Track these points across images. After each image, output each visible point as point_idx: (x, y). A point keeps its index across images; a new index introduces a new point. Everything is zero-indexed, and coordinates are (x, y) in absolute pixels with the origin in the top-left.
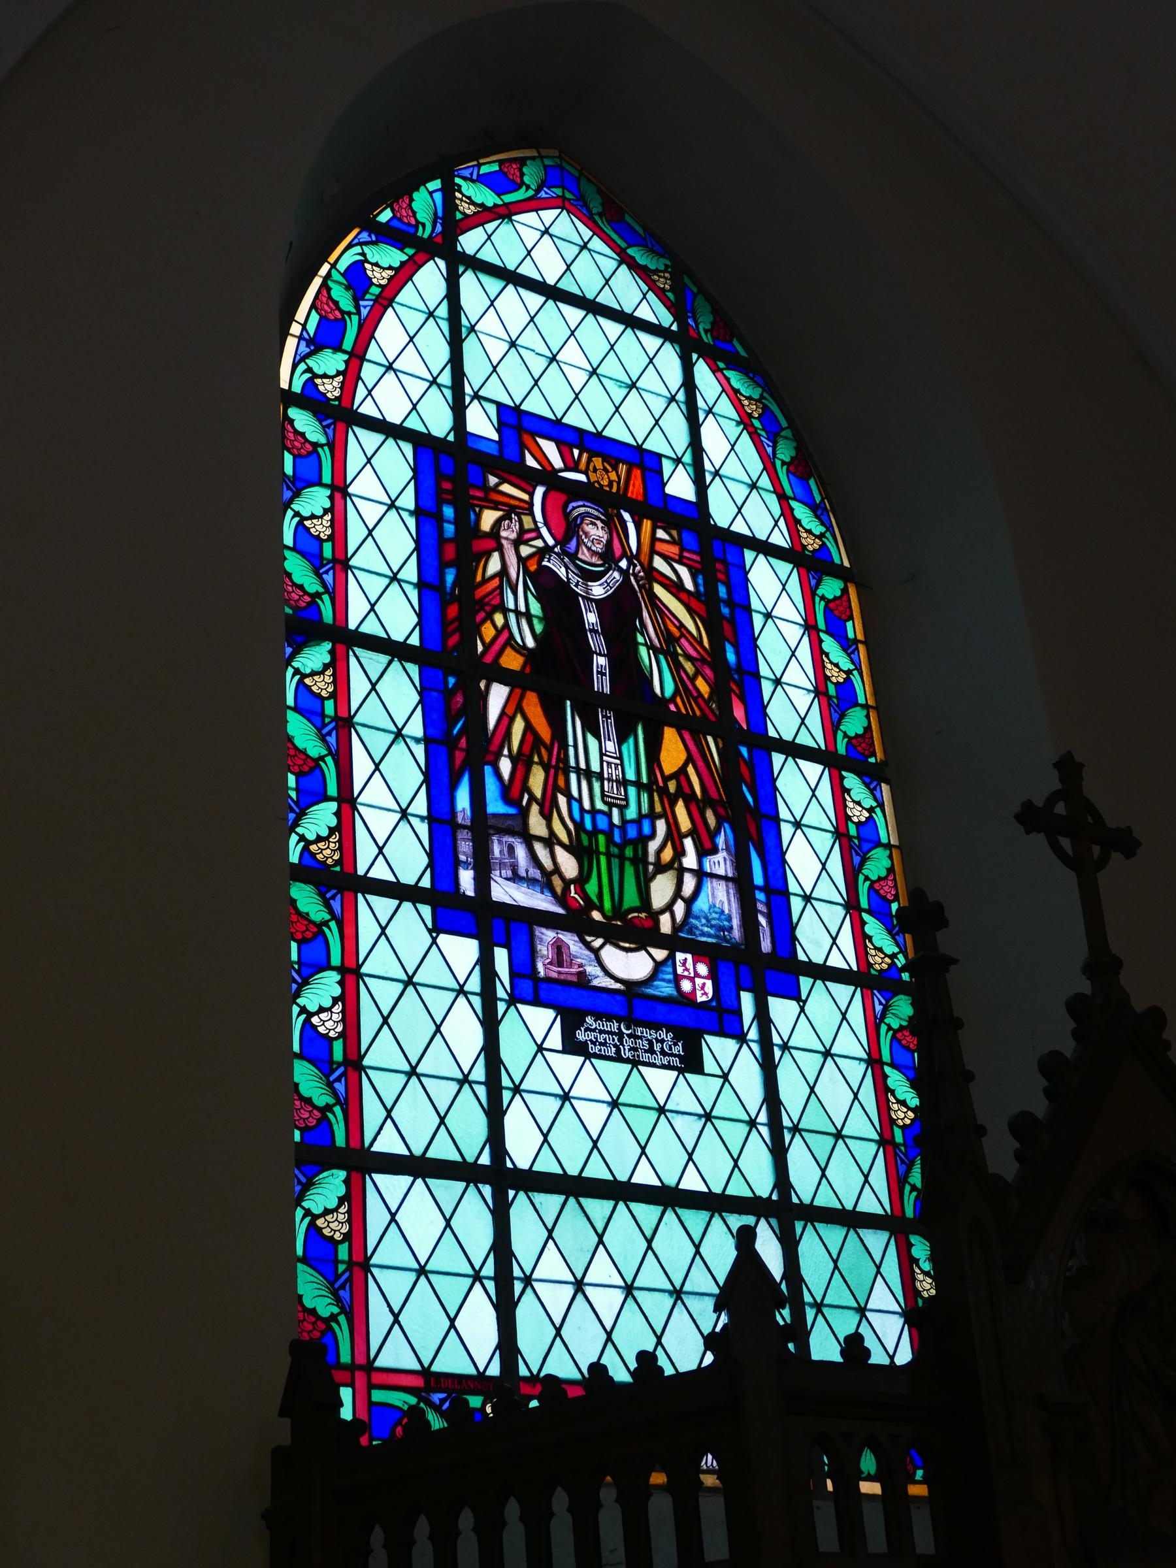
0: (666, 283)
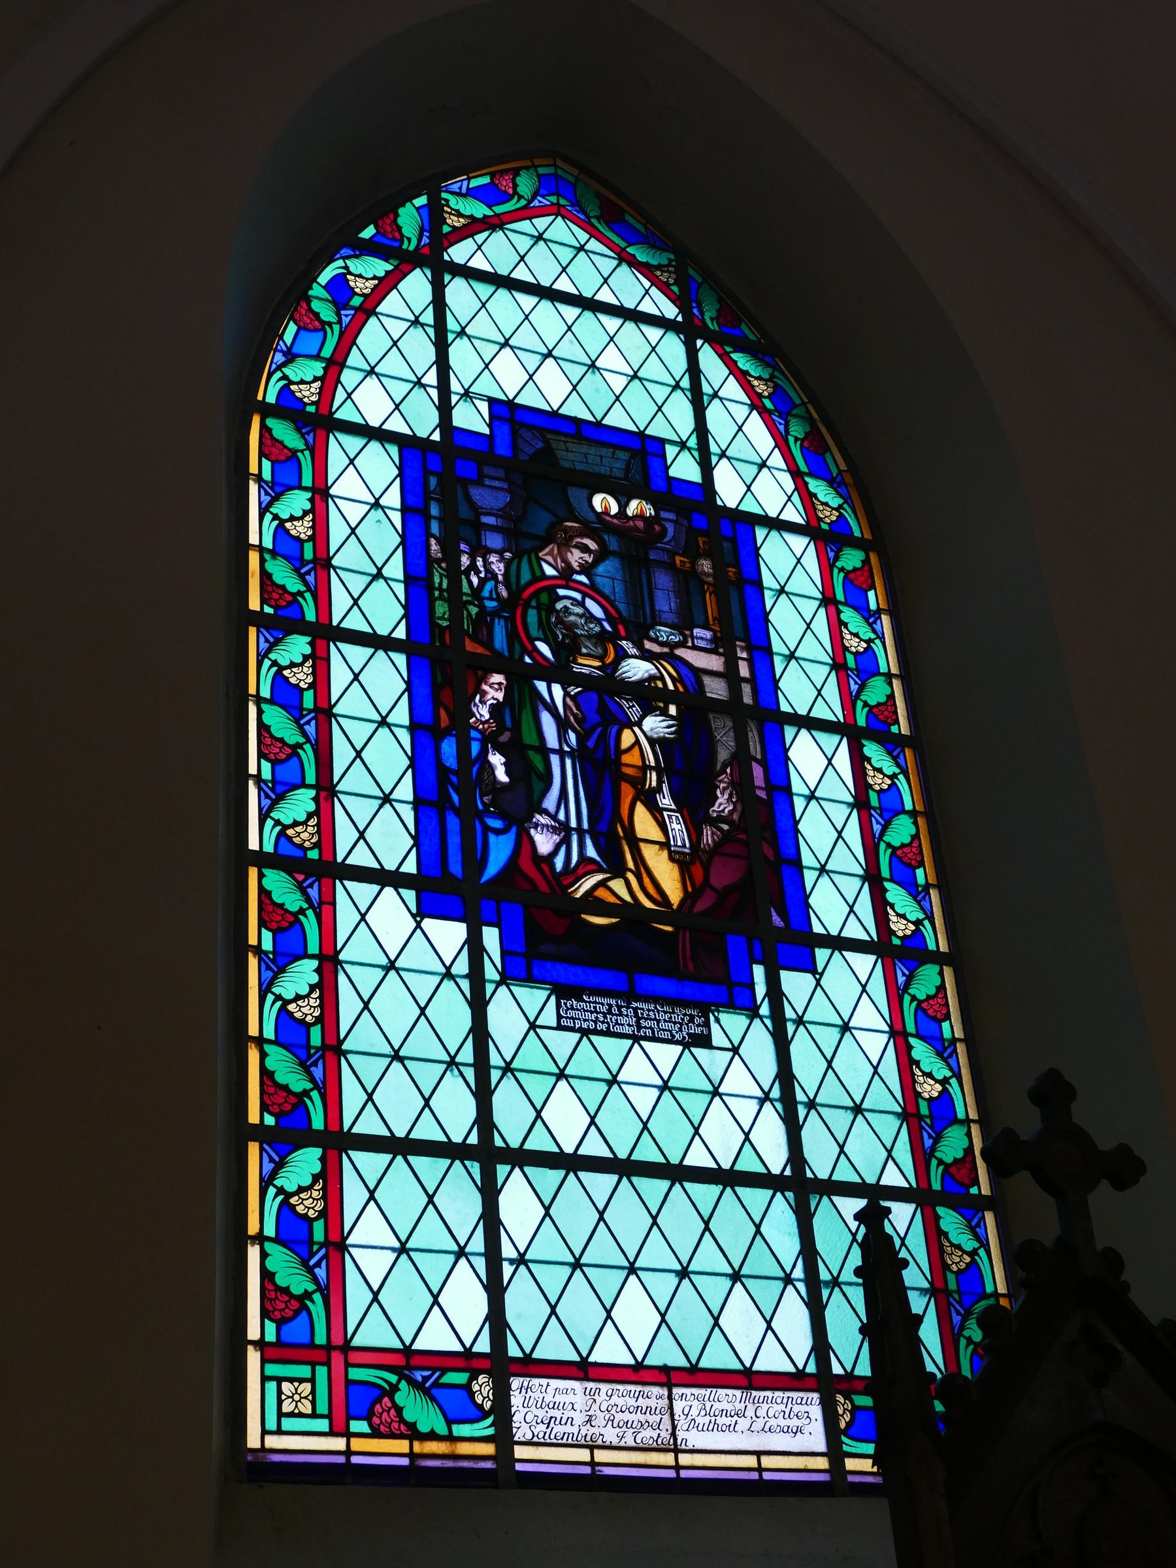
0: (670, 277)
